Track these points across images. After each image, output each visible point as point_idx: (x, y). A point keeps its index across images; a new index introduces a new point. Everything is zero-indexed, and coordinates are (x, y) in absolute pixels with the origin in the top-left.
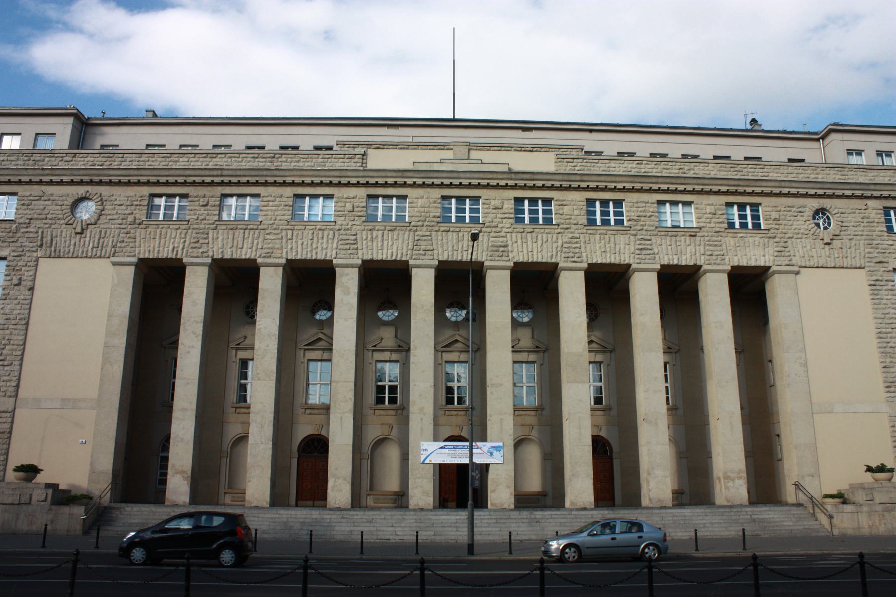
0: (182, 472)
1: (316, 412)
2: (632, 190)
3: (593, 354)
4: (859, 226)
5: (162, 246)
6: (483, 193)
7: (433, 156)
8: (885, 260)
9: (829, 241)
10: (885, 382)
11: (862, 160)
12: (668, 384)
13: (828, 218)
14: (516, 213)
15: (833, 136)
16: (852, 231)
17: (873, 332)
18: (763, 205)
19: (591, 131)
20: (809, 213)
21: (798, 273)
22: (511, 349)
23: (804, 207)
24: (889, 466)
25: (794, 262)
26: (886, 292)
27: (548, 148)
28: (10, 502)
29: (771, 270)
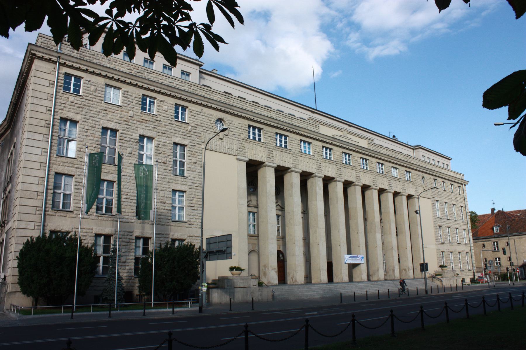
0: (274, 269)
1: (252, 238)
3: (278, 211)
5: (257, 153)
6: (160, 97)
9: (222, 138)
12: (280, 225)
13: (223, 124)
14: (64, 84)
15: (420, 150)
18: (84, 79)
19: (365, 131)
20: (214, 119)
22: (246, 204)
24: (242, 268)
25: (246, 156)
28: (243, 286)
29: (264, 164)
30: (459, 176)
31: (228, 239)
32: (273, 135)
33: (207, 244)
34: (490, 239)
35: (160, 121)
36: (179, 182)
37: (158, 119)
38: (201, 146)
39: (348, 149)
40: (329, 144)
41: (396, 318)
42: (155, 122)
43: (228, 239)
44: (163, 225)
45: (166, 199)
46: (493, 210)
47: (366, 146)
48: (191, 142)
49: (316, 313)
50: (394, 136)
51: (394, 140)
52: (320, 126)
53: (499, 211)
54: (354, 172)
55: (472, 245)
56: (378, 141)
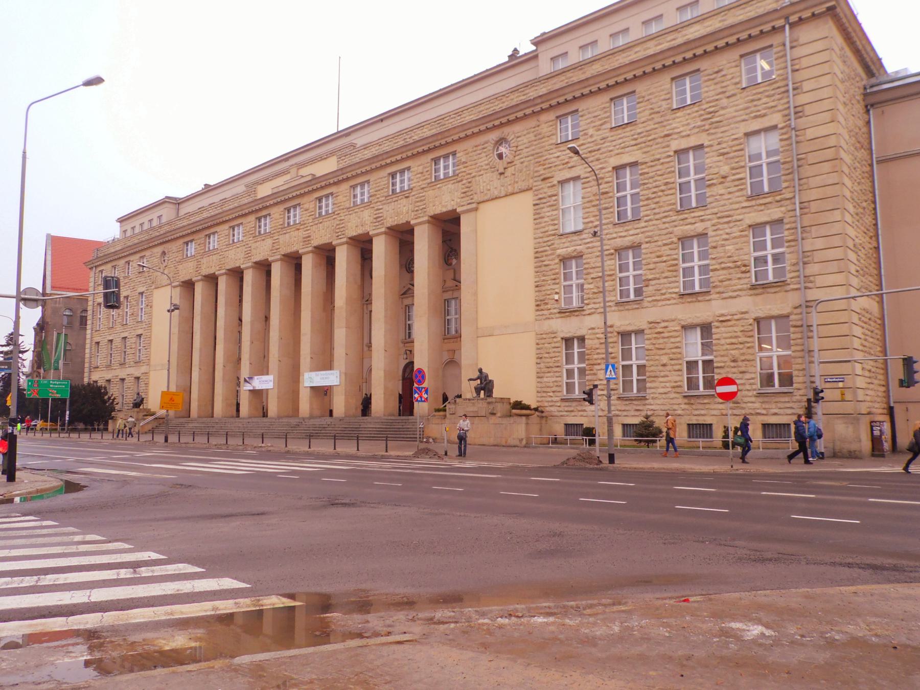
2: (372, 170)
4: (532, 145)
7: (279, 182)
8: (549, 175)
10: (536, 301)
11: (666, 24)
16: (525, 152)
17: (531, 253)
19: (318, 146)
20: (490, 146)
21: (476, 209)
23: (486, 143)
26: (549, 209)
27: (332, 153)
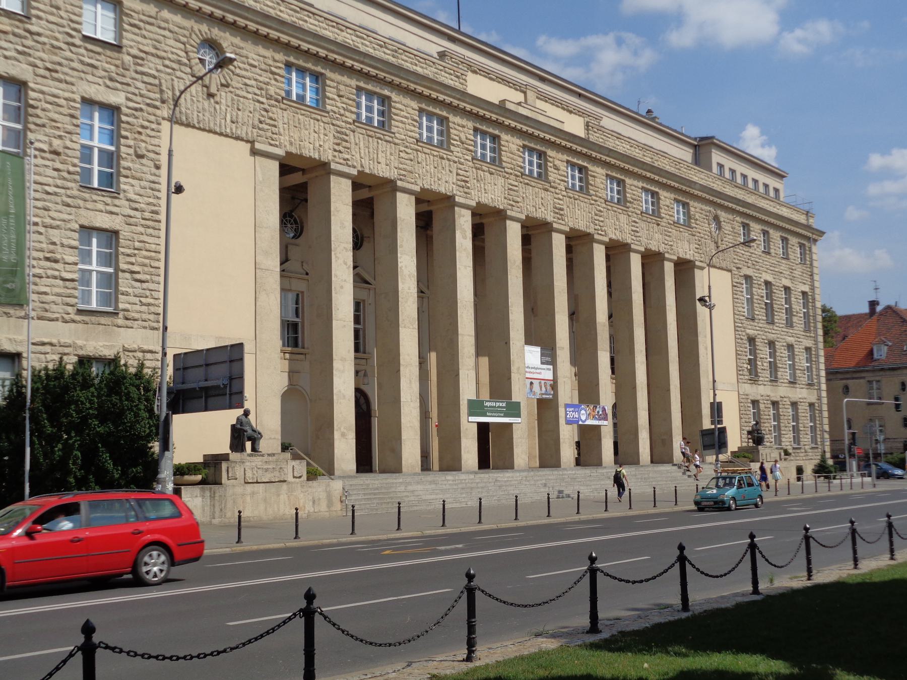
5: (312, 140)
19: (580, 95)
30: (802, 219)
31: (233, 355)
32: (351, 93)
33: (176, 369)
34: (863, 375)
35: (39, 34)
36: (100, 206)
37: (34, 28)
38: (158, 112)
39: (541, 140)
40: (491, 120)
41: (691, 564)
42: (25, 38)
43: (233, 355)
44: (52, 320)
45: (60, 249)
46: (873, 304)
47: (580, 132)
48: (128, 99)
49: (460, 546)
50: (649, 111)
51: (648, 121)
52: (469, 73)
53: (889, 308)
54: (549, 196)
55: (824, 387)
56: (610, 122)
